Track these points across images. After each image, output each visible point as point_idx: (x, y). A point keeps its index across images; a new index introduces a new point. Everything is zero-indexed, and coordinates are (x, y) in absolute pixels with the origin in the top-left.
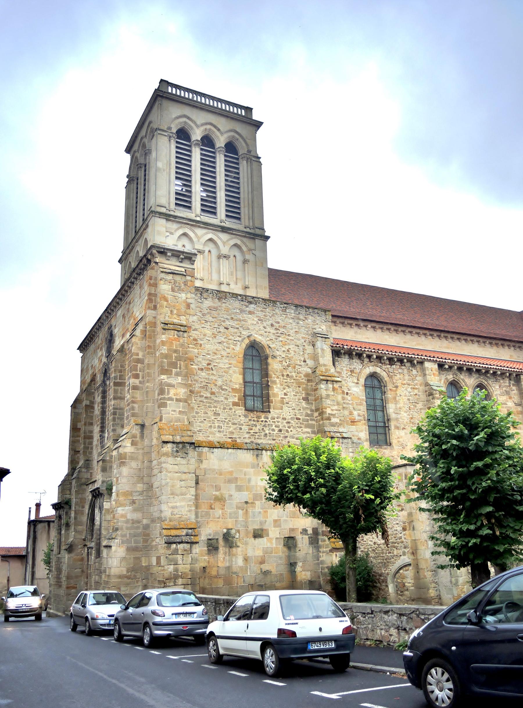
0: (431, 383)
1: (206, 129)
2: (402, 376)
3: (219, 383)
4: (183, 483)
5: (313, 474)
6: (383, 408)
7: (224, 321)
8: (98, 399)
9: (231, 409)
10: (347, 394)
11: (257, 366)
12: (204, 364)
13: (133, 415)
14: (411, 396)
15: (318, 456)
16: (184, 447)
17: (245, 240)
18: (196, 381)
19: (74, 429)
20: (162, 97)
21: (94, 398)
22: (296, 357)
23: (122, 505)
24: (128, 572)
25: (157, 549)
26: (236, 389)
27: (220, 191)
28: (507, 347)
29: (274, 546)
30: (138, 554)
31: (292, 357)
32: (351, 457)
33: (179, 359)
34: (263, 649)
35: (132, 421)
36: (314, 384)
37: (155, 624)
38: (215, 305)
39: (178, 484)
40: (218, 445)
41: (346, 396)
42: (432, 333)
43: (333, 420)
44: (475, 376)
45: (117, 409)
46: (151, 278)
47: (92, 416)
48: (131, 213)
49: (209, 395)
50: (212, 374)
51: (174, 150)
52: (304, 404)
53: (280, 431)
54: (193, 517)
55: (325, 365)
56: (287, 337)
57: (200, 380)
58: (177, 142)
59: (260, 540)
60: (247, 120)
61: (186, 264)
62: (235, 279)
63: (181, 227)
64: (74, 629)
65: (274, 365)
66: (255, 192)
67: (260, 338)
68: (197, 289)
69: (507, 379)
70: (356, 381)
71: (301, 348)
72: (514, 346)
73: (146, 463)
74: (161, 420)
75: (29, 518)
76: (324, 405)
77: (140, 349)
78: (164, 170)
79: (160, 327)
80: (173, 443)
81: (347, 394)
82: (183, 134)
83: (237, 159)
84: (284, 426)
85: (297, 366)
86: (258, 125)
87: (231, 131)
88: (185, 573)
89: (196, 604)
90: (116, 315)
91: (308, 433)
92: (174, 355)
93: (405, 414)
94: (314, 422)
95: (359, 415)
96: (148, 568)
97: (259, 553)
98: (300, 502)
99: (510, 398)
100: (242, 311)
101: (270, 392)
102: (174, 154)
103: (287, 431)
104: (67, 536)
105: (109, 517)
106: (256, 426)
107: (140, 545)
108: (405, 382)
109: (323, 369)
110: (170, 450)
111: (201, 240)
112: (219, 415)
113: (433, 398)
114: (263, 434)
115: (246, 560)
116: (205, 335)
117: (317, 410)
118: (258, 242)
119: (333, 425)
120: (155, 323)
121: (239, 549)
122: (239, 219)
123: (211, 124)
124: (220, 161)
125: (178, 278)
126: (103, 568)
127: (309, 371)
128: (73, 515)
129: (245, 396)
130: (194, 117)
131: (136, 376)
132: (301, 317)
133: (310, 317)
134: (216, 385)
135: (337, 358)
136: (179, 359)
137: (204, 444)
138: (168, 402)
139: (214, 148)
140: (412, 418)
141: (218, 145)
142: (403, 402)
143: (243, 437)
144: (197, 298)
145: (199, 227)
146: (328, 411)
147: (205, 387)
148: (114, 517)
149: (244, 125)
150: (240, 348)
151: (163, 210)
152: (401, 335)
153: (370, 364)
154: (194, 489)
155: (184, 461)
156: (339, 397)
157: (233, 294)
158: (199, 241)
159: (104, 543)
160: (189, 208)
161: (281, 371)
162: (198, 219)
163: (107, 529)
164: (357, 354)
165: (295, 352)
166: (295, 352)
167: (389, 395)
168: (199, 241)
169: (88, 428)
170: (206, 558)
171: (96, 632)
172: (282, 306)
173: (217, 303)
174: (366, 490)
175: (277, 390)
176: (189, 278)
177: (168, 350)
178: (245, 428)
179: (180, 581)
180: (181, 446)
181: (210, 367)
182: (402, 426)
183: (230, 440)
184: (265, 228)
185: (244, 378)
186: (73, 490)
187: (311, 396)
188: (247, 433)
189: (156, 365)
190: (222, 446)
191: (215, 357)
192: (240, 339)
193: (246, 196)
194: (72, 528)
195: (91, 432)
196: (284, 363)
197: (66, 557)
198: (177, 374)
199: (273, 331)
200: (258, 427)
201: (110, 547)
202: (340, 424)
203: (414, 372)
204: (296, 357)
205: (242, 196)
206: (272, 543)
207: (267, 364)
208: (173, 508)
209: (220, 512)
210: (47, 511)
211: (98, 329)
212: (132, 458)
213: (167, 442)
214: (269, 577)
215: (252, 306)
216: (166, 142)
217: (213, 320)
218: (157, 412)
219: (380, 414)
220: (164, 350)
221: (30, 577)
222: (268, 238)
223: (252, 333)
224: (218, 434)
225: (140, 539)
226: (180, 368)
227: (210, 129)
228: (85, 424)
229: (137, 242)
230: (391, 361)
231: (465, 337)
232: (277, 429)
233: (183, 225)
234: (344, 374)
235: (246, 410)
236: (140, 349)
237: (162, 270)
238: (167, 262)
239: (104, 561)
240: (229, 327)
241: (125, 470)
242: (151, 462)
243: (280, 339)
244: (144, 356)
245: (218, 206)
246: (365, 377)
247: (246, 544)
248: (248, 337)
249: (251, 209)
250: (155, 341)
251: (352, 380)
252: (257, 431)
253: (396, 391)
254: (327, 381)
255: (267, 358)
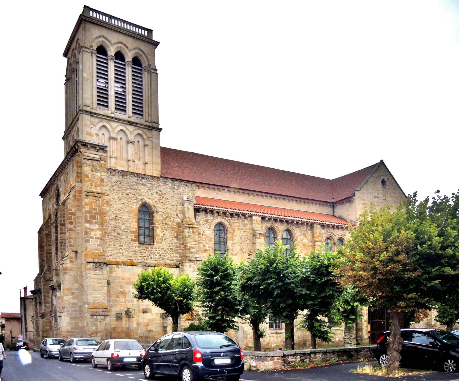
0: (256, 229)
1: (118, 47)
2: (238, 224)
3: (123, 228)
4: (100, 284)
5: (155, 286)
6: (225, 243)
7: (126, 190)
8: (53, 230)
9: (130, 243)
10: (203, 234)
11: (147, 217)
12: (113, 216)
13: (71, 246)
14: (243, 236)
15: (159, 278)
16: (100, 265)
17: (145, 130)
18: (108, 226)
19: (41, 247)
20: (86, 21)
21: (51, 229)
22: (172, 212)
23: (66, 295)
24: (71, 329)
25: (86, 318)
26: (133, 231)
27: (128, 94)
28: (315, 204)
29: (155, 317)
30: (77, 321)
31: (169, 213)
32: (175, 278)
33: (96, 214)
34: (107, 361)
35: (70, 249)
36: (182, 229)
37: (75, 353)
38: (120, 180)
39: (97, 285)
40: (122, 264)
41: (201, 236)
42: (266, 195)
43: (192, 250)
44: (285, 224)
45: (63, 240)
46: (78, 162)
47: (50, 241)
48: (69, 104)
49: (116, 235)
50: (118, 222)
51: (95, 62)
52: (175, 240)
53: (160, 255)
54: (106, 302)
55: (189, 218)
56: (166, 200)
57: (111, 226)
58: (98, 57)
59: (147, 314)
60: (148, 40)
61: (101, 153)
62: (138, 157)
63: (101, 121)
64: (42, 356)
65: (157, 217)
66: (153, 96)
67: (149, 200)
68: (108, 169)
69: (306, 226)
70: (209, 227)
71: (175, 207)
72: (319, 204)
73: (79, 273)
74: (86, 249)
75: (21, 296)
76: (187, 241)
77: (73, 206)
78: (88, 79)
79: (84, 194)
80: (94, 263)
81: (203, 234)
82: (102, 50)
83: (141, 70)
84: (163, 253)
85: (172, 218)
86: (156, 44)
87: (136, 48)
88: (102, 330)
89: (96, 345)
90: (60, 179)
91: (177, 257)
92: (94, 211)
93: (238, 247)
94: (181, 251)
95: (209, 247)
96: (83, 328)
97: (146, 321)
98: (150, 299)
99: (306, 237)
100: (137, 184)
101: (155, 233)
102: (95, 66)
103: (164, 256)
104: (41, 309)
105: (60, 301)
106: (145, 253)
107: (78, 316)
108: (240, 228)
109: (188, 220)
110: (92, 266)
111: (115, 131)
112: (122, 246)
113: (255, 238)
114: (149, 257)
115: (138, 324)
116: (113, 199)
117: (183, 244)
118: (154, 132)
119: (191, 253)
120: (81, 191)
121: (134, 319)
122: (142, 115)
123: (122, 43)
124: (128, 72)
125: (95, 163)
126: (58, 327)
127: (180, 221)
128: (43, 298)
129: (139, 235)
130: (109, 38)
131: (71, 223)
132: (176, 187)
133: (182, 188)
134: (120, 229)
135: (197, 213)
136: (96, 214)
137: (113, 263)
138: (91, 239)
139: (124, 62)
140: (242, 249)
141: (127, 60)
142: (237, 239)
143: (137, 259)
144: (108, 175)
145: (113, 121)
146: (189, 245)
147: (114, 230)
148: (62, 301)
149: (146, 44)
150: (136, 207)
151: (88, 109)
152: (247, 195)
153: (218, 217)
154: (106, 288)
155: (100, 273)
156: (196, 237)
157: (132, 173)
158: (113, 131)
159: (58, 315)
160: (107, 107)
161: (162, 221)
162: (113, 115)
163: (59, 307)
164: (210, 211)
165: (171, 209)
166: (171, 209)
167: (229, 235)
168: (113, 131)
169: (49, 248)
170: (115, 323)
171: (51, 357)
172: (164, 180)
173: (121, 178)
174: (180, 295)
175: (159, 232)
176: (102, 162)
177: (90, 208)
178: (139, 254)
179: (99, 334)
180: (98, 264)
181: (117, 218)
182: (235, 253)
183: (129, 261)
184: (159, 122)
185: (138, 225)
186: (42, 284)
187: (179, 236)
188: (140, 257)
189: (83, 217)
190: (124, 264)
191: (120, 212)
192: (136, 201)
193: (147, 98)
194: (43, 305)
195: (51, 250)
196: (164, 216)
197: (41, 321)
198: (96, 223)
199: (157, 196)
200: (147, 253)
201: (61, 317)
202: (196, 253)
203: (246, 222)
204: (172, 212)
205: (144, 98)
206: (153, 316)
207: (153, 217)
208: (94, 297)
209: (123, 299)
210: (29, 294)
211: (51, 185)
212: (71, 270)
213: (90, 262)
214: (151, 333)
215: (144, 180)
216: (89, 57)
217: (119, 189)
218: (84, 244)
219: (223, 246)
220: (87, 208)
221: (24, 330)
222: (161, 129)
223: (144, 197)
224: (122, 257)
225: (78, 313)
226: (97, 219)
227: (121, 47)
228: (46, 245)
229: (73, 128)
230: (232, 215)
231: (287, 198)
232: (158, 255)
233: (102, 120)
234: (202, 222)
235: (139, 243)
236: (73, 206)
237: (84, 157)
238: (88, 151)
239: (59, 323)
240: (129, 194)
241: (67, 277)
242: (82, 272)
243: (162, 201)
244: (75, 211)
245: (127, 105)
246: (214, 225)
247: (138, 316)
248: (141, 200)
249: (150, 108)
250: (82, 202)
251: (206, 226)
252: (146, 255)
253: (233, 233)
254: (189, 227)
255: (153, 213)
